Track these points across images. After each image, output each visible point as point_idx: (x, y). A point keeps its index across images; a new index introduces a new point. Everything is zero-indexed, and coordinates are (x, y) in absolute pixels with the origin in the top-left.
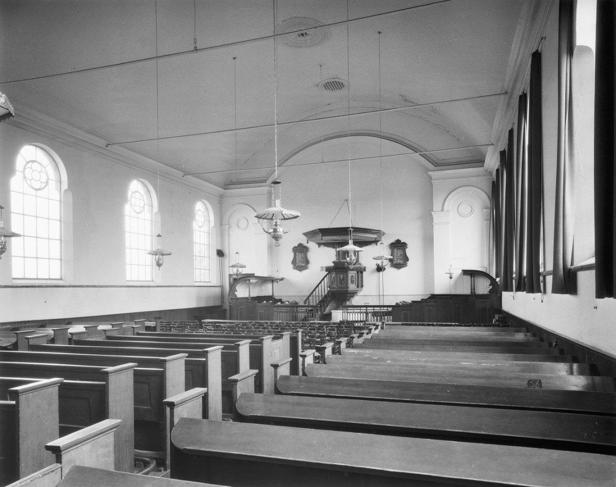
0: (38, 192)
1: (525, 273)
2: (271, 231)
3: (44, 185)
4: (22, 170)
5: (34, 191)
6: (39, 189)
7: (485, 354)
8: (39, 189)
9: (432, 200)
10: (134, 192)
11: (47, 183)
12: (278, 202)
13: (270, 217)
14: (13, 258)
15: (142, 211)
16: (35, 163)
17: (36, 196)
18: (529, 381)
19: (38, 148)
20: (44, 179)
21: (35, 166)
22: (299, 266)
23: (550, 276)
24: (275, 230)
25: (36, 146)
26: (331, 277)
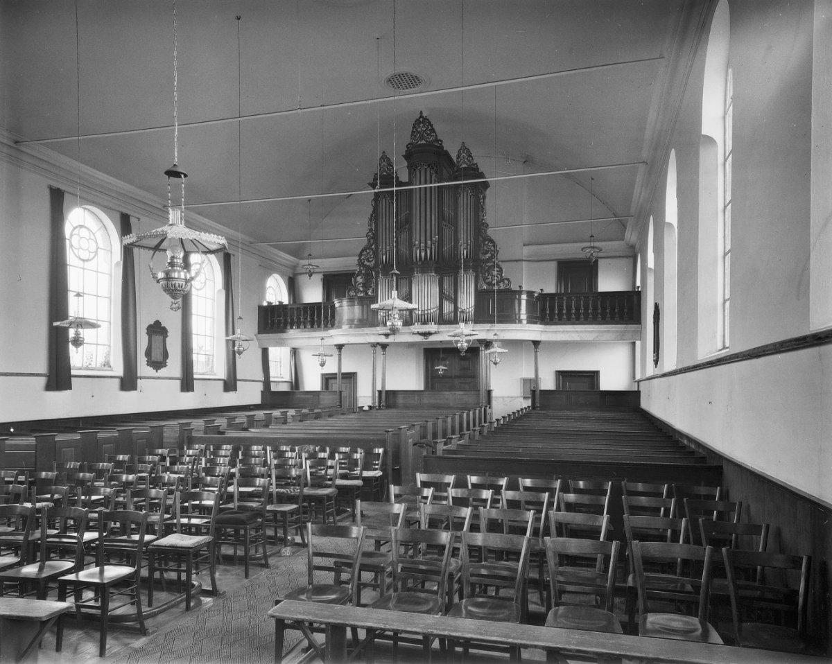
0: (86, 263)
1: (333, 597)
2: (161, 275)
3: (92, 255)
4: (99, 250)
5: (82, 262)
6: (87, 260)
7: (720, 357)
8: (87, 260)
9: (807, 190)
10: (77, 227)
11: (96, 252)
12: (174, 215)
13: (155, 242)
14: (139, 381)
15: (93, 258)
16: (83, 229)
17: (83, 269)
18: (508, 280)
19: (86, 212)
20: (93, 248)
21: (84, 232)
22: (154, 362)
23: (267, 532)
24: (168, 278)
25: (85, 209)
26: (359, 531)
